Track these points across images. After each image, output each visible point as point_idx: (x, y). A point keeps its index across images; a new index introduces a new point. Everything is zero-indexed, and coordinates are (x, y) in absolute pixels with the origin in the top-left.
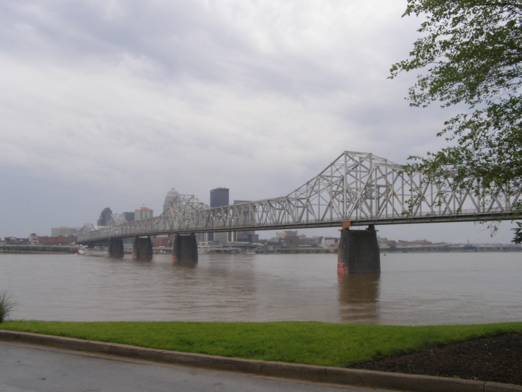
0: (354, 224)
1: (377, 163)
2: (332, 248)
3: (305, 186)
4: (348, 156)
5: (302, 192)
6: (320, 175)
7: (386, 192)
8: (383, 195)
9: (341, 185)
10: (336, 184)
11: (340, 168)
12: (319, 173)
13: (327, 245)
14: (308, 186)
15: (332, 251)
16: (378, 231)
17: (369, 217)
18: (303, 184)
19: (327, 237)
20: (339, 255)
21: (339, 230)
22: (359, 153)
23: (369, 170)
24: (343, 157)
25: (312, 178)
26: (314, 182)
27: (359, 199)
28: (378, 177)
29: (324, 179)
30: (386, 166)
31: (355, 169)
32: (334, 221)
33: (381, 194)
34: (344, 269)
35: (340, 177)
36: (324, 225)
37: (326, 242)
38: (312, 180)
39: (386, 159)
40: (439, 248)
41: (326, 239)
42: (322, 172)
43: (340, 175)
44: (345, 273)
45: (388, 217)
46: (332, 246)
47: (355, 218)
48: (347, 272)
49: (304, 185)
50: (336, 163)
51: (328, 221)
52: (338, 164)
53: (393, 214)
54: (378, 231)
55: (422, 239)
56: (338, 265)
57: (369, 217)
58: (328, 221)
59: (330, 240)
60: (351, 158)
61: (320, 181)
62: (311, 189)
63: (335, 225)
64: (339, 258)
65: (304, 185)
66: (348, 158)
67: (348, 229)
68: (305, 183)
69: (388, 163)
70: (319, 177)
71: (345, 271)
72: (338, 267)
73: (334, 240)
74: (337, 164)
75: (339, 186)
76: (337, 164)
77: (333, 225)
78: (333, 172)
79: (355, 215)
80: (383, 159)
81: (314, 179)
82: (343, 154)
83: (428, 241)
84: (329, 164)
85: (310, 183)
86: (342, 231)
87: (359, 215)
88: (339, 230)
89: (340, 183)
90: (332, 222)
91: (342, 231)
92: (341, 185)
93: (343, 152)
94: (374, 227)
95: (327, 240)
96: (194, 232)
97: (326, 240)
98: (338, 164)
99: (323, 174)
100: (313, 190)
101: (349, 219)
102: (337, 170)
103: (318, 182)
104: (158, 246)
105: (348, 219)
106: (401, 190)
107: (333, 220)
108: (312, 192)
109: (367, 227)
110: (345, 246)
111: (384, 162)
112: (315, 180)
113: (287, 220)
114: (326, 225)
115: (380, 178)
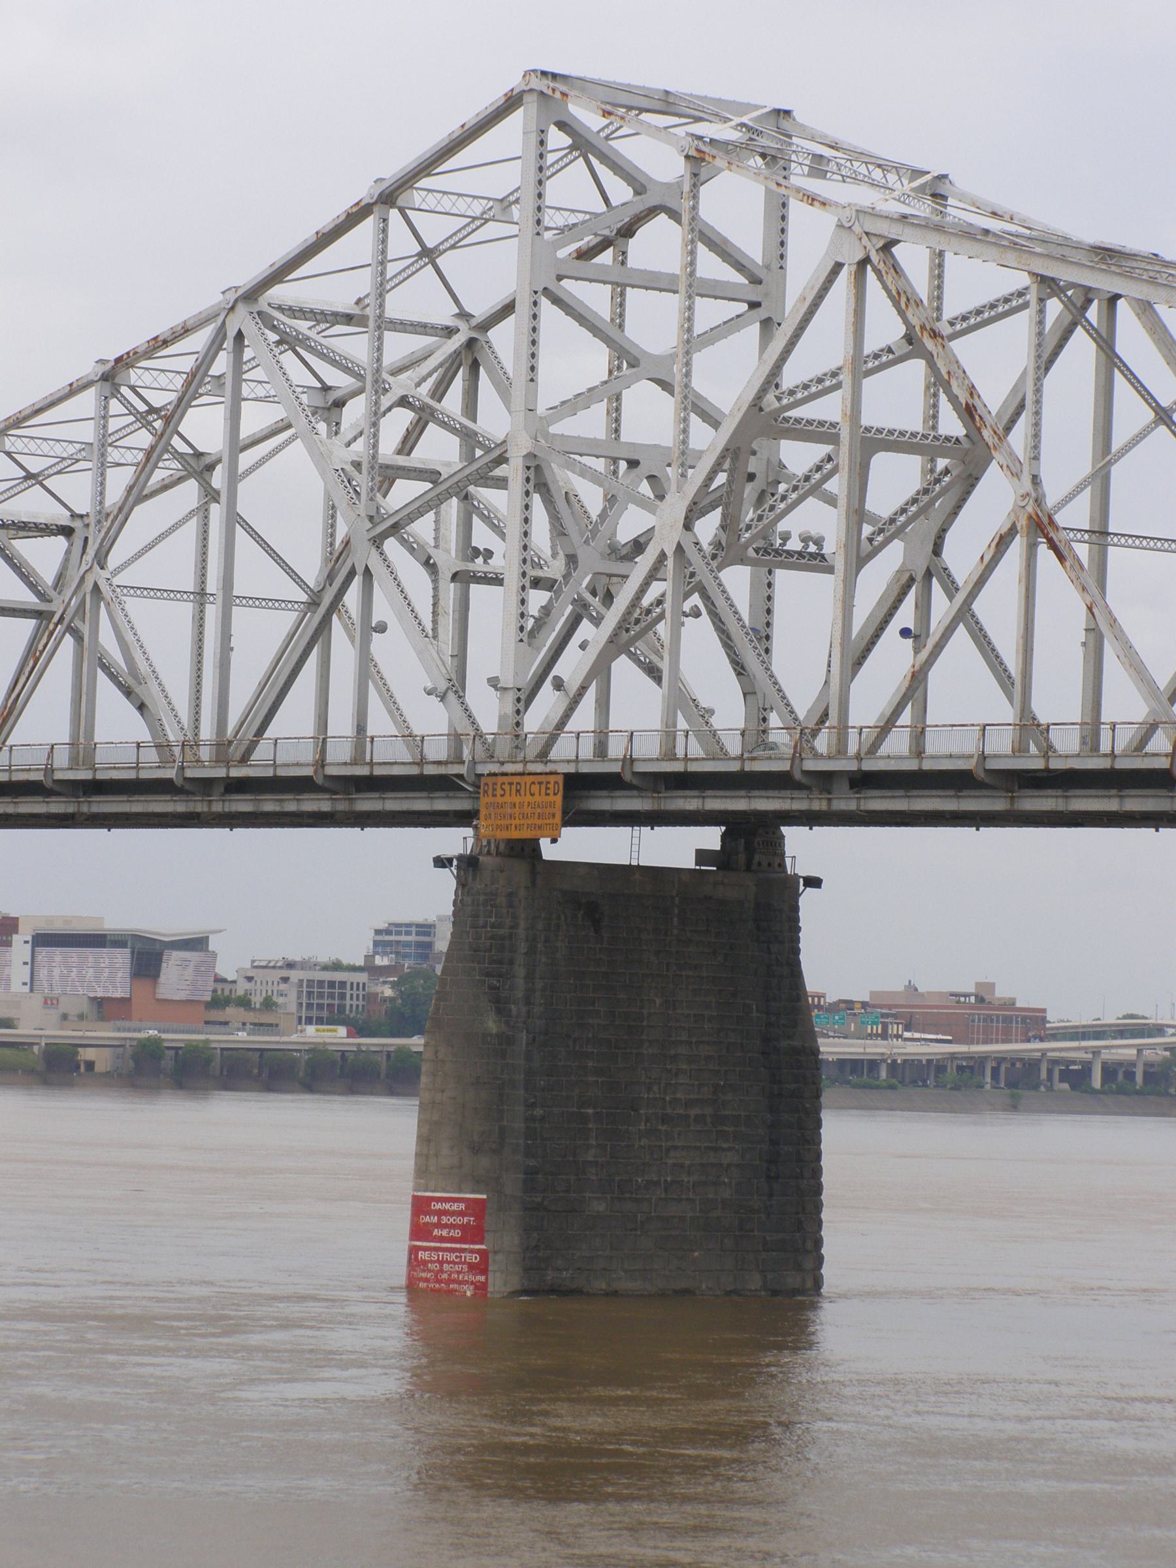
0: (602, 803)
1: (873, 213)
2: (106, 1032)
3: (87, 401)
4: (562, 126)
5: (34, 465)
6: (252, 295)
7: (921, 502)
8: (891, 529)
9: (453, 402)
10: (403, 402)
11: (454, 243)
12: (247, 275)
13: (50, 1002)
14: (115, 406)
15: (102, 1060)
16: (813, 882)
17: (734, 746)
18: (59, 384)
19: (58, 927)
20: (422, 1108)
21: (441, 862)
22: (667, 104)
23: (756, 281)
24: (513, 128)
25: (161, 328)
26: (187, 364)
27: (663, 556)
28: (871, 345)
29: (289, 341)
30: (937, 241)
31: (606, 257)
32: (378, 771)
33: (873, 519)
34: (471, 1252)
35: (449, 332)
36: (269, 805)
37: (43, 973)
38: (159, 344)
39: (942, 177)
40: (1109, 1071)
41: (43, 940)
42: (278, 275)
43: (444, 314)
44: (481, 1288)
45: (616, 749)
46: (105, 1008)
47: (307, 754)
48: (499, 1282)
49: (74, 390)
50: (424, 183)
51: (49, 770)
52: (447, 203)
53: (669, 735)
54: (813, 882)
55: (892, 983)
56: (420, 1206)
57: (734, 746)
58: (49, 770)
59: (90, 954)
60: (582, 145)
61: (248, 354)
62: (144, 439)
63: (393, 803)
64: (425, 1140)
65: (74, 390)
66: (557, 139)
67: (527, 850)
68: (87, 368)
69: (956, 212)
70: (241, 320)
71: (481, 1268)
72: (419, 1231)
73: (122, 958)
74: (431, 201)
75: (425, 417)
76: (431, 201)
77: (367, 803)
78: (392, 269)
79: (308, 728)
80: (917, 173)
81: (186, 331)
82: (512, 102)
83: (1010, 1004)
84: (362, 190)
85: (134, 376)
86: (468, 865)
87: (341, 724)
88: (441, 862)
89: (439, 392)
90: (84, 775)
91: (468, 865)
92: (453, 402)
93: (513, 81)
94: (776, 845)
95: (58, 954)
96: (1135, 754)
97: (43, 952)
98: (447, 203)
99: (280, 293)
100: (168, 445)
101: (543, 756)
102: (428, 254)
103: (222, 364)
104: (290, 1035)
105: (531, 751)
106: (1085, 500)
107: (100, 757)
108: (151, 457)
109: (711, 837)
110: (492, 1025)
111: (923, 209)
112: (199, 340)
113: (341, 724)
114: (269, 807)
115: (888, 358)
